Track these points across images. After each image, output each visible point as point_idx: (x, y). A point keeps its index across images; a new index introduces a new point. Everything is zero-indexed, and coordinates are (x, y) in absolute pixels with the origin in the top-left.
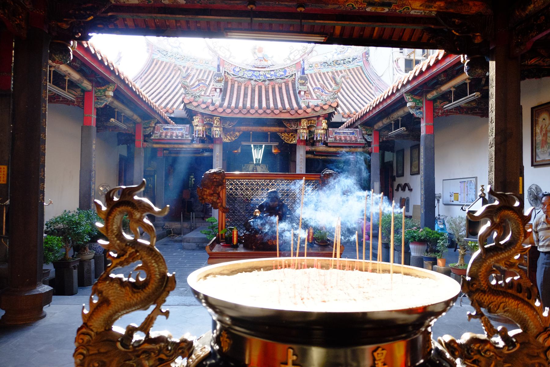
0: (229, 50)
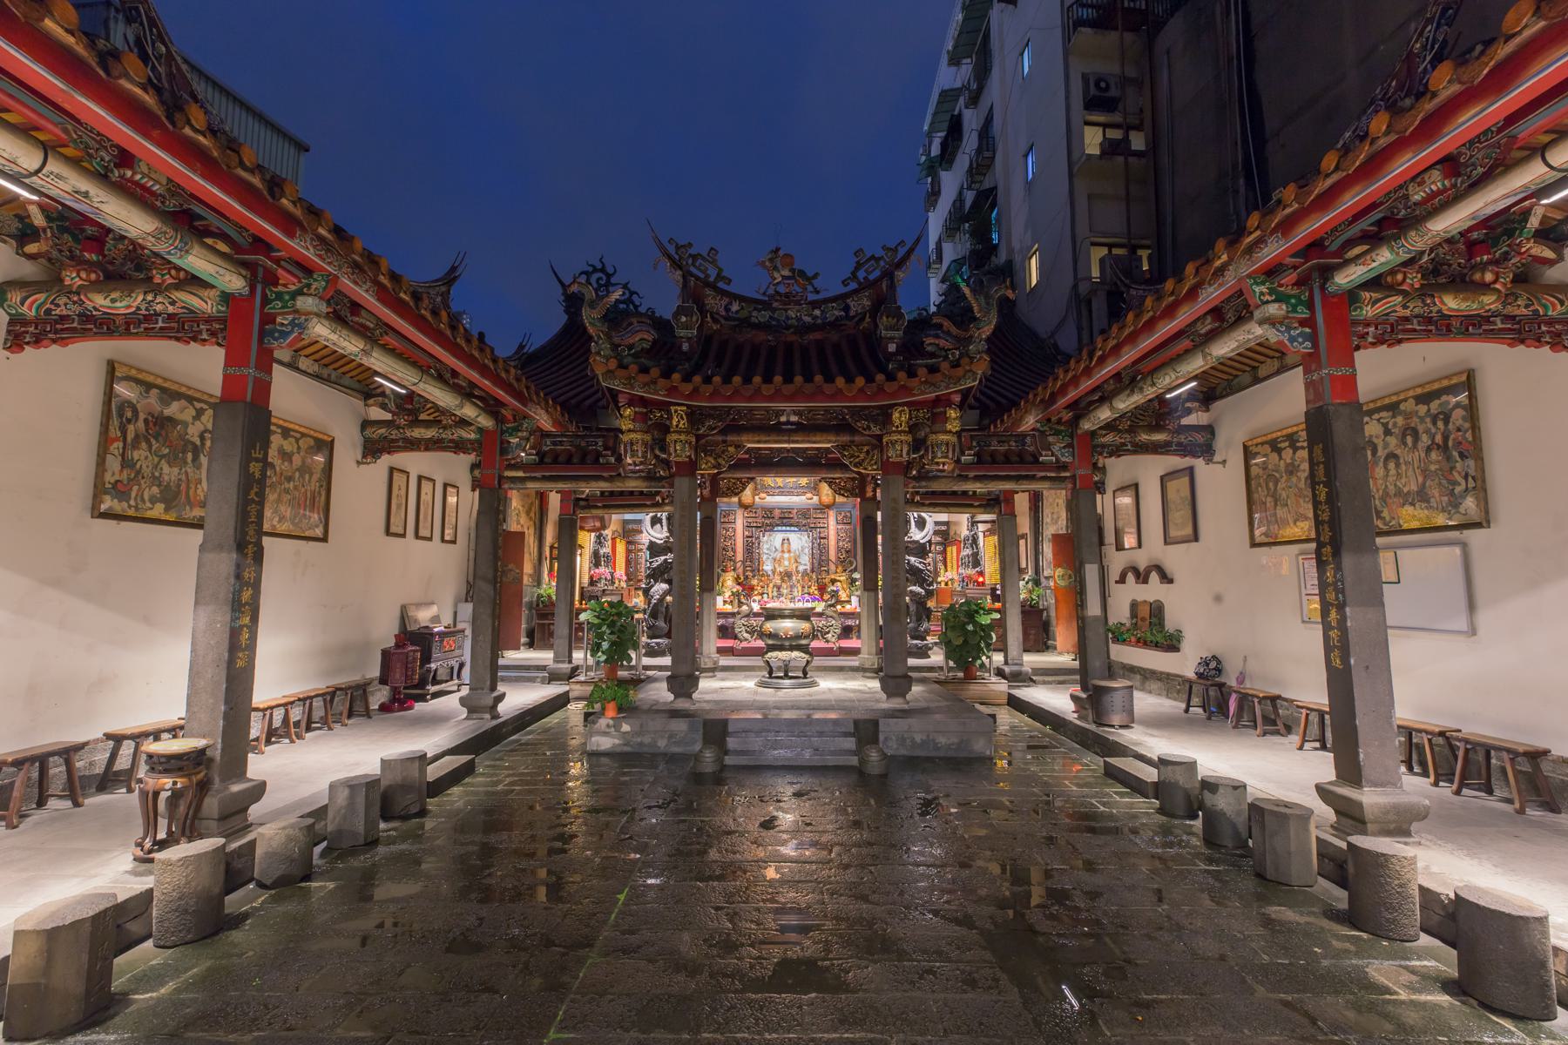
0: (714, 262)
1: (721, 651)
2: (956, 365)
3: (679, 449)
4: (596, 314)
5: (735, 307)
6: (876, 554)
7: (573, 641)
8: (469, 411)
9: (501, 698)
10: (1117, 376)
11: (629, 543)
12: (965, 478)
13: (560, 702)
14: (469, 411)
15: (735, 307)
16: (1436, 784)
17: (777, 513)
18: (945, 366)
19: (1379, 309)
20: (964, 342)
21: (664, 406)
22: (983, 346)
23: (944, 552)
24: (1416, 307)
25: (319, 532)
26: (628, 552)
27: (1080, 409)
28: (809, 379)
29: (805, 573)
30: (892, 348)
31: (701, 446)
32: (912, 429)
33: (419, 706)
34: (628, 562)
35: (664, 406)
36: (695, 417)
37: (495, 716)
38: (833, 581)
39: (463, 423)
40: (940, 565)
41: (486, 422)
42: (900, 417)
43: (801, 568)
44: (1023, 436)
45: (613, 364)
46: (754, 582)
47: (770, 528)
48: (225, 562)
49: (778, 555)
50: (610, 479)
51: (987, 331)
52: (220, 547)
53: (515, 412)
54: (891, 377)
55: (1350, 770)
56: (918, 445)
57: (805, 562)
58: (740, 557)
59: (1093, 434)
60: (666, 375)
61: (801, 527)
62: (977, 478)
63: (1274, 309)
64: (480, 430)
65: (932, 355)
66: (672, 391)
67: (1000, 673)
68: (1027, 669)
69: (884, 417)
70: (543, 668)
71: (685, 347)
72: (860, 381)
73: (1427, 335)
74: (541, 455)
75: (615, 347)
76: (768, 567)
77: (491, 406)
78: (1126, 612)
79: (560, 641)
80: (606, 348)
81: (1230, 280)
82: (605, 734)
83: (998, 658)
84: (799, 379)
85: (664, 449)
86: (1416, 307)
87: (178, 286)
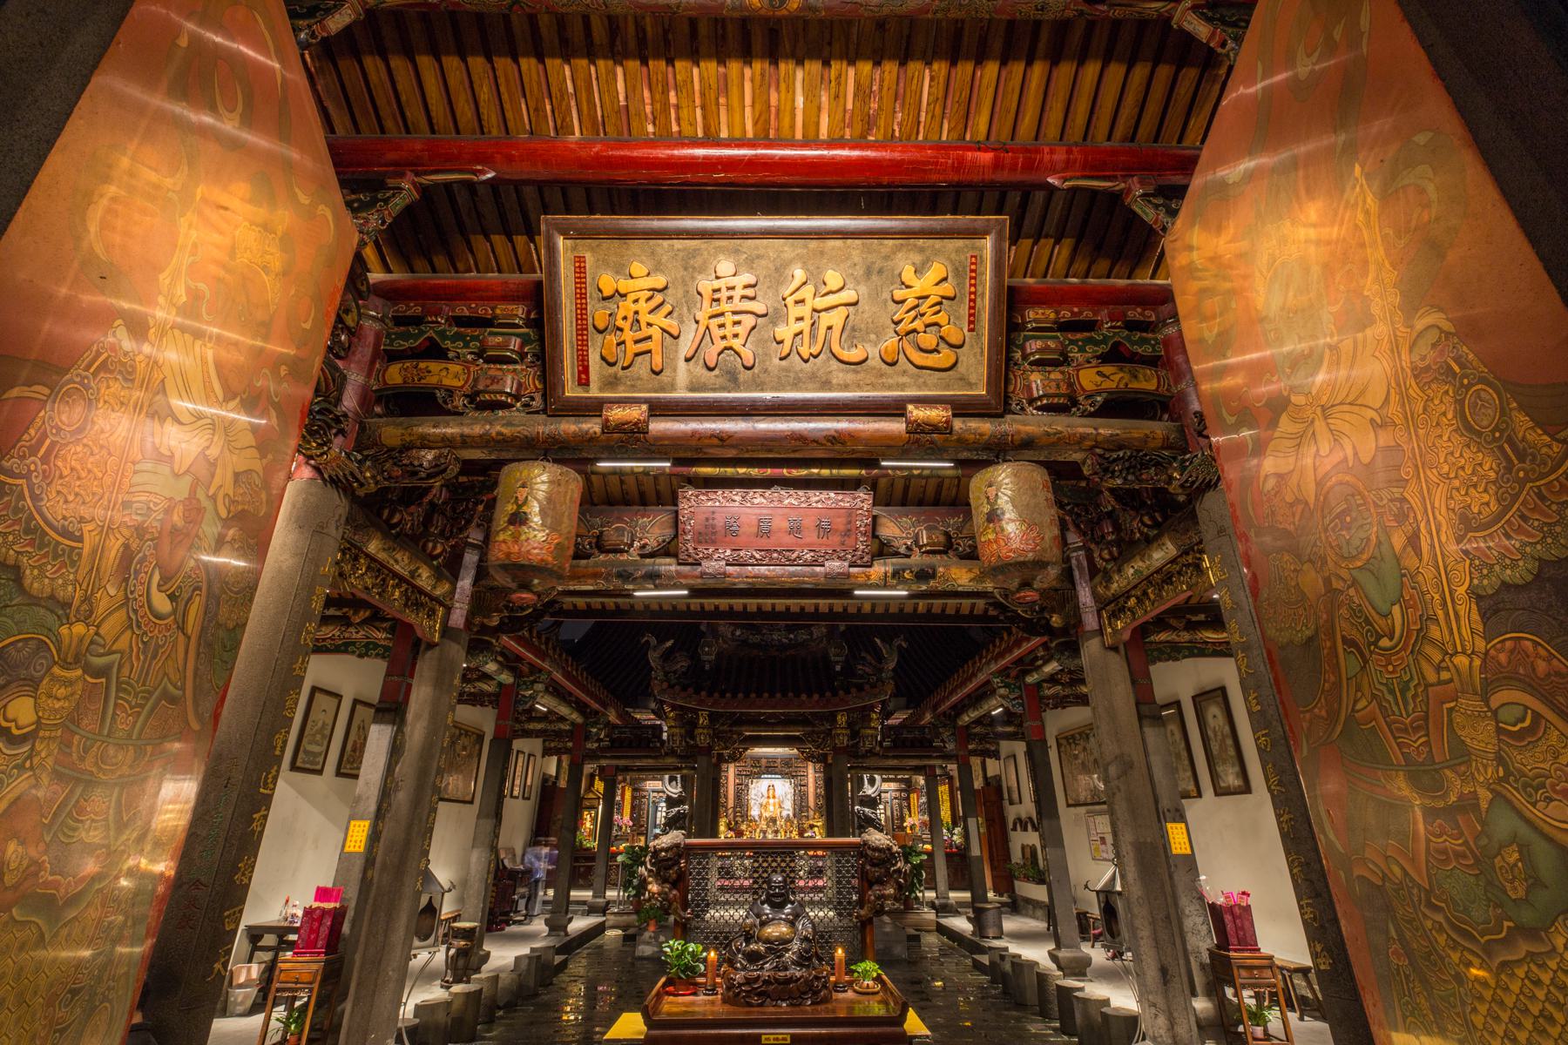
1: (722, 889)
2: (873, 686)
3: (702, 738)
4: (656, 655)
5: (738, 633)
6: (838, 807)
7: (609, 883)
8: (564, 710)
9: (570, 920)
10: (969, 696)
11: (634, 790)
12: (887, 757)
13: (599, 929)
14: (564, 710)
15: (738, 633)
16: (1301, 1019)
17: (764, 762)
18: (867, 687)
19: (1052, 691)
20: (881, 670)
21: (695, 711)
22: (890, 674)
23: (908, 799)
24: (1068, 691)
25: (299, 764)
26: (634, 798)
27: (959, 709)
28: (784, 695)
29: (788, 819)
30: (838, 668)
31: (717, 736)
32: (850, 725)
33: (508, 929)
34: (633, 808)
35: (695, 711)
36: (713, 717)
37: (567, 934)
38: (812, 827)
39: (562, 719)
40: (906, 811)
41: (575, 717)
42: (842, 719)
43: (784, 814)
44: (924, 727)
45: (665, 685)
46: (744, 827)
47: (758, 776)
48: (488, 824)
49: (764, 801)
50: (656, 758)
51: (892, 665)
52: (487, 816)
53: (532, 666)
54: (835, 694)
55: (1058, 946)
56: (855, 735)
57: (788, 808)
58: (731, 803)
59: (967, 727)
60: (697, 692)
61: (785, 775)
62: (895, 757)
63: (1002, 691)
64: (573, 724)
65: (861, 677)
66: (701, 702)
67: (932, 905)
68: (952, 901)
69: (832, 718)
70: (584, 903)
71: (707, 667)
72: (816, 697)
73: (1077, 704)
74: (612, 741)
75: (666, 674)
76: (754, 812)
77: (581, 707)
78: (1020, 854)
79: (598, 881)
80: (661, 675)
81: (981, 677)
82: (648, 943)
83: (931, 895)
84: (778, 695)
85: (693, 738)
86: (1068, 691)
87: (478, 679)
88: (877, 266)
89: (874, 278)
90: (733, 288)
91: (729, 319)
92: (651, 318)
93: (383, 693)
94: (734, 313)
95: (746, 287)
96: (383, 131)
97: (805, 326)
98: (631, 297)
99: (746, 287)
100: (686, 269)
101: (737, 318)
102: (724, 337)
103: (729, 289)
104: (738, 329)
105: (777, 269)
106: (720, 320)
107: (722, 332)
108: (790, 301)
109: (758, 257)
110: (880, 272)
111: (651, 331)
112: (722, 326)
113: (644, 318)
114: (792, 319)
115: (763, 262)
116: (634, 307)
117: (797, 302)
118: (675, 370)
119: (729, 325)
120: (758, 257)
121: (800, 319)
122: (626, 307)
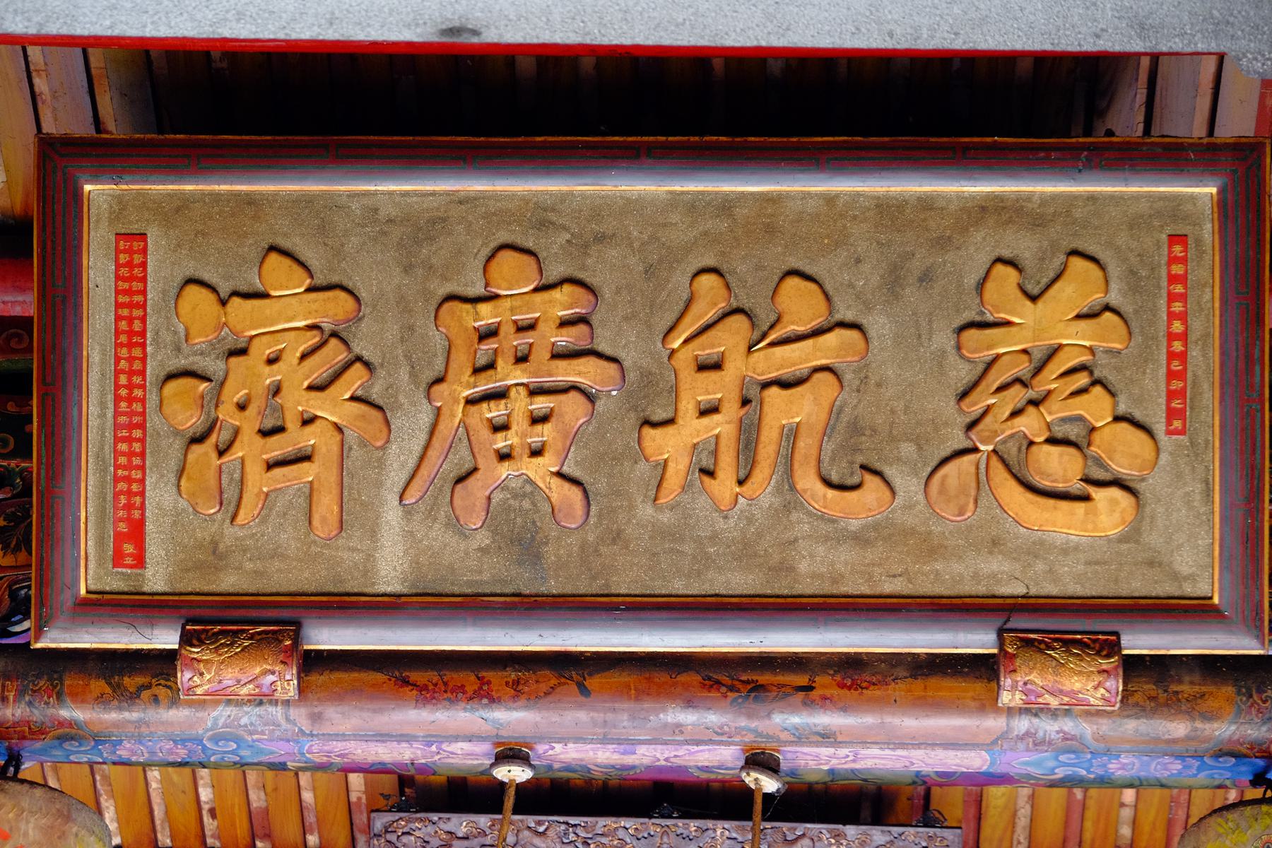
88: (917, 266)
89: (910, 293)
90: (531, 327)
91: (520, 405)
92: (320, 406)
93: (366, 784)
94: (535, 392)
95: (564, 323)
96: (29, 629)
97: (722, 425)
98: (262, 350)
99: (564, 323)
100: (408, 269)
101: (542, 404)
102: (504, 456)
103: (522, 328)
104: (546, 432)
105: (649, 271)
106: (494, 411)
107: (501, 442)
108: (685, 359)
109: (601, 238)
110: (926, 278)
111: (309, 438)
112: (500, 427)
113: (297, 401)
114: (687, 407)
115: (613, 253)
116: (270, 376)
117: (703, 367)
118: (373, 534)
119: (519, 423)
120: (601, 238)
121: (709, 410)
122: (247, 378)
